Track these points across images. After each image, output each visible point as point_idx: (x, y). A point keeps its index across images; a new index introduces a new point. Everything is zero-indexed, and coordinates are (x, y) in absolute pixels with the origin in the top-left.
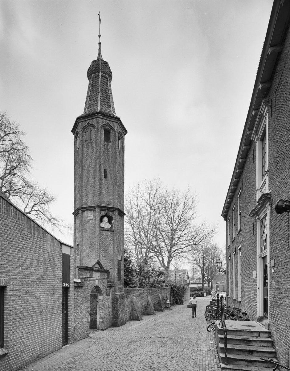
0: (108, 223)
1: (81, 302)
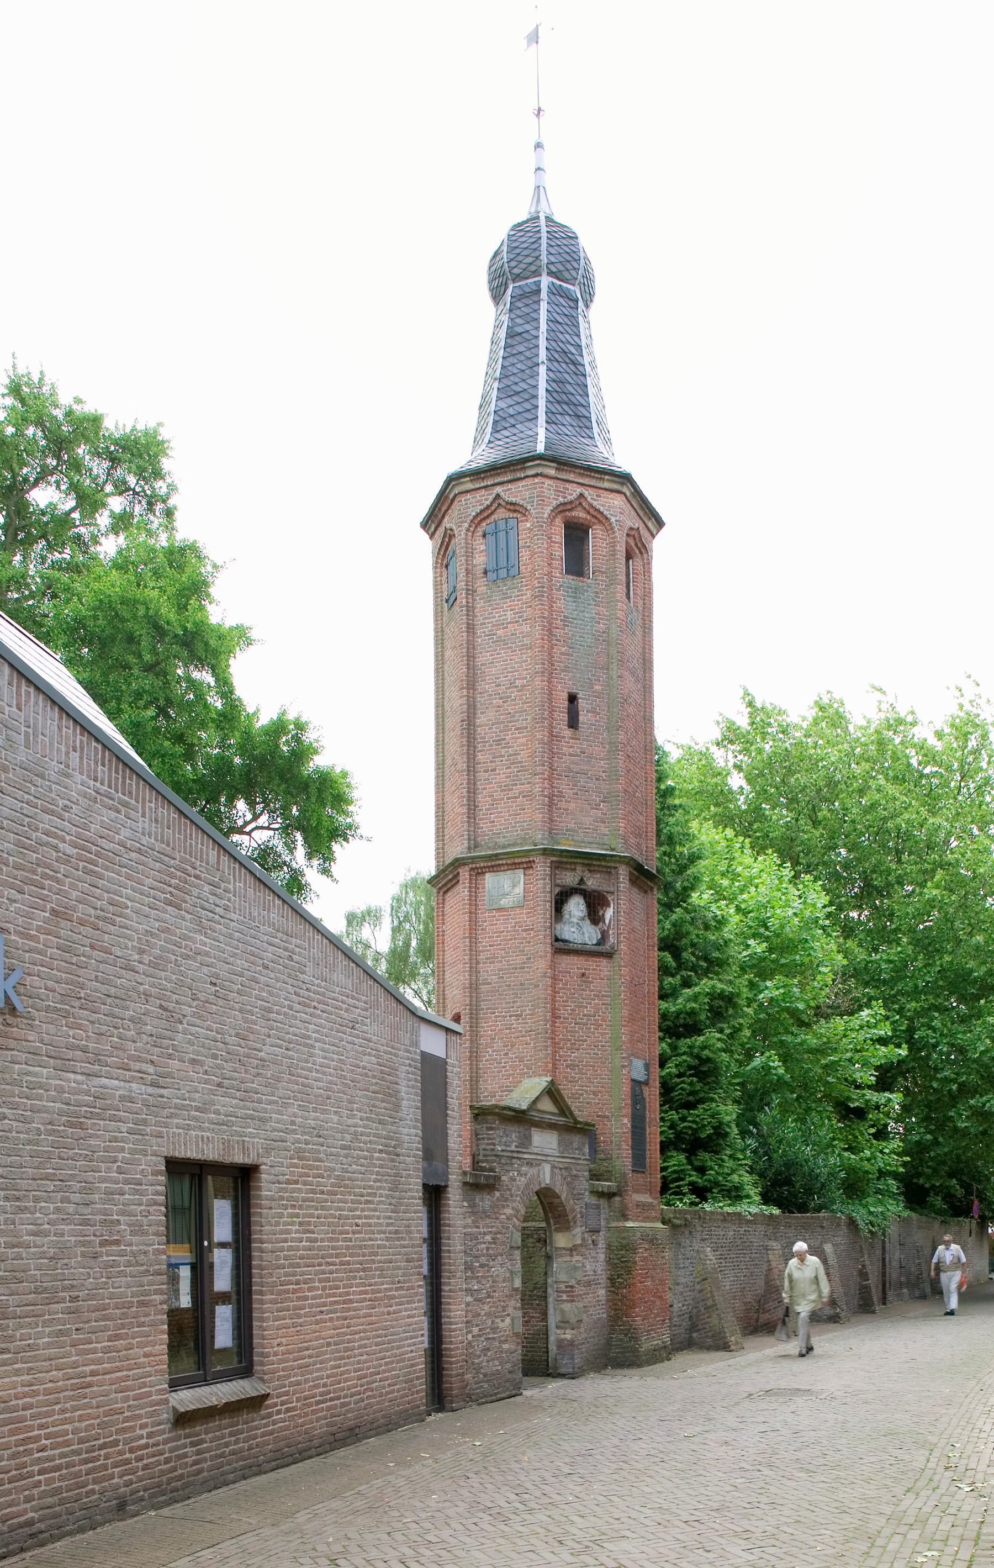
0: (588, 922)
1: (488, 1249)
